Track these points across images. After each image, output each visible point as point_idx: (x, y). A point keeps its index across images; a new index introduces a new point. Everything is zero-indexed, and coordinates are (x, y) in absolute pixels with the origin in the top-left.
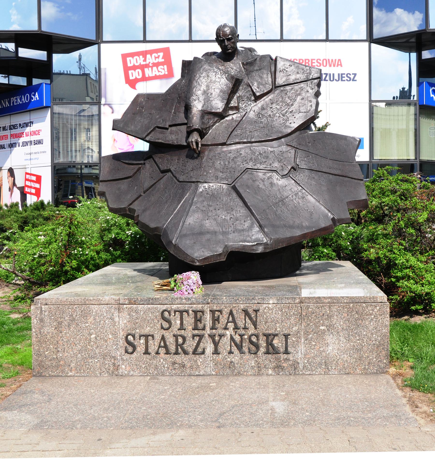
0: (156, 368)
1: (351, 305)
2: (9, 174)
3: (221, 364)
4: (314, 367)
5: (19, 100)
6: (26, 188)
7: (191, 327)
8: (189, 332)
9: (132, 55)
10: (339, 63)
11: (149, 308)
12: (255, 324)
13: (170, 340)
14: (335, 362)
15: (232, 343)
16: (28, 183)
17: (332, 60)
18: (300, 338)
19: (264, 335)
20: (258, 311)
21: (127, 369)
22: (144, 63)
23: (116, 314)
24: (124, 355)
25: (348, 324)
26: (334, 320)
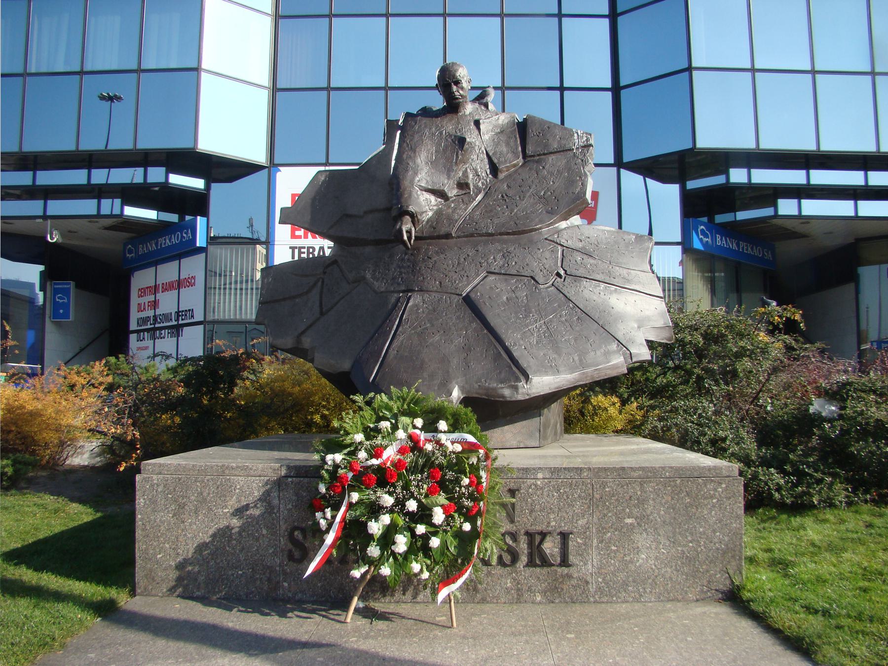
4: (615, 589)
14: (650, 581)
18: (590, 538)
19: (527, 533)
24: (286, 565)
25: (673, 515)
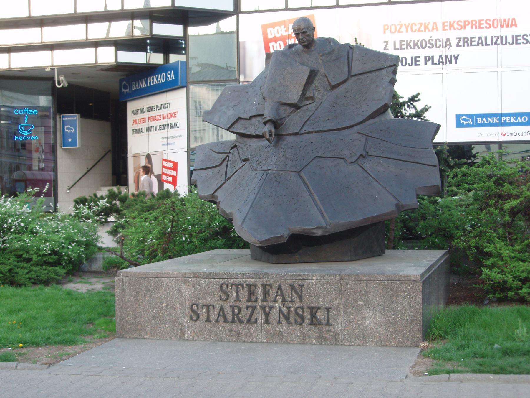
0: (216, 334)
1: (386, 283)
2: (147, 161)
3: (271, 333)
5: (155, 80)
6: (163, 176)
7: (245, 299)
8: (243, 304)
9: (273, 25)
10: (513, 23)
11: (210, 282)
12: (300, 297)
13: (228, 311)
14: (371, 335)
15: (281, 315)
16: (165, 171)
17: (505, 20)
18: (340, 311)
20: (303, 285)
21: (192, 334)
22: (286, 34)
23: (183, 286)
26: (371, 295)
